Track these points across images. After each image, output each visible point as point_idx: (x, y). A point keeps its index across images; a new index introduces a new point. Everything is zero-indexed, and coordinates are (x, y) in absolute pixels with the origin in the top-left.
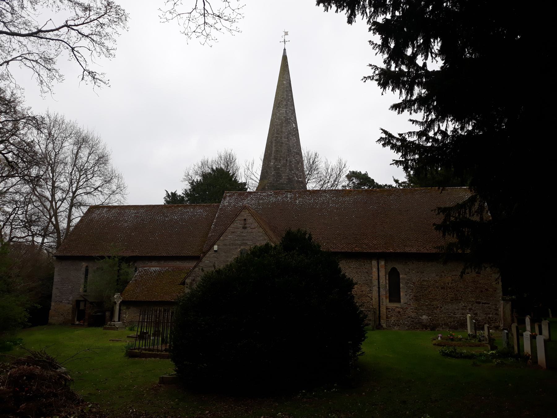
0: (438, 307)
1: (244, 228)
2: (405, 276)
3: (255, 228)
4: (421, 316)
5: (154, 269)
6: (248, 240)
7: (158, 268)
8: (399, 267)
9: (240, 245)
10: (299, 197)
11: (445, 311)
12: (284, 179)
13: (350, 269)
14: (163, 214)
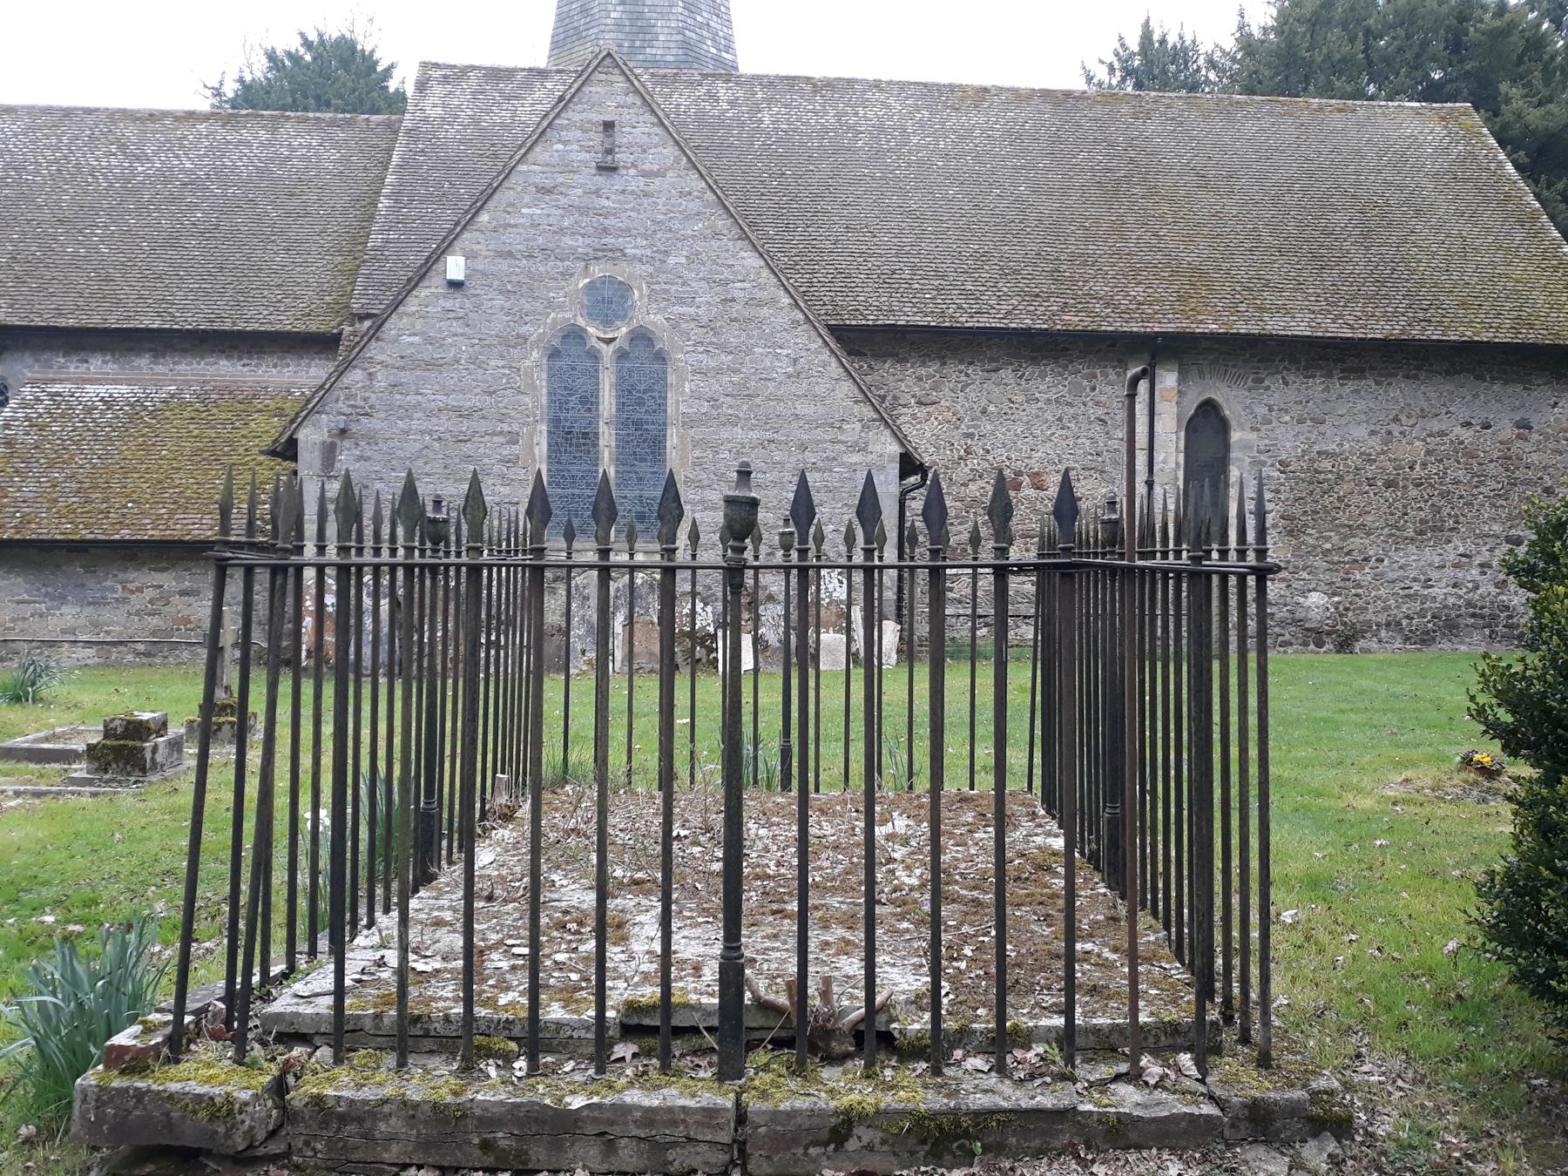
0: (1366, 559)
2: (1254, 435)
3: (660, 174)
4: (1304, 593)
5: (102, 390)
6: (626, 232)
7: (124, 389)
8: (1232, 399)
9: (587, 260)
10: (769, 101)
11: (1392, 575)
12: (664, 46)
13: (1033, 409)
14: (123, 147)
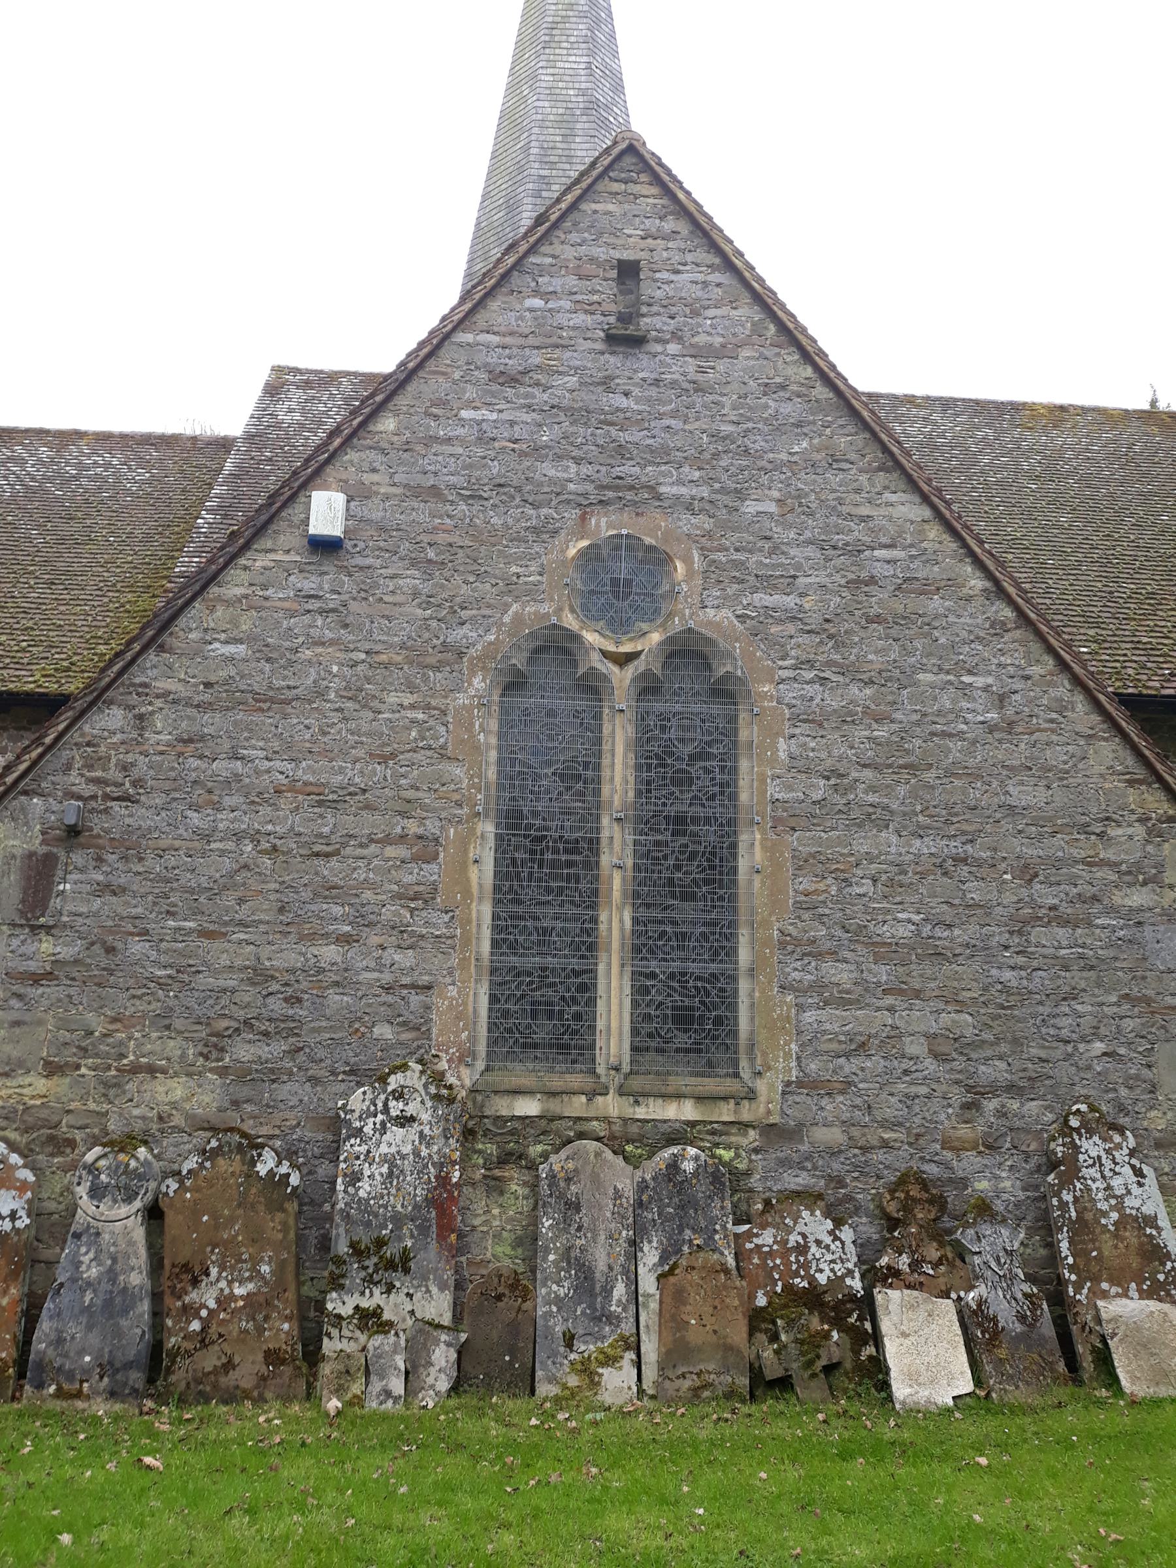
1: (625, 339)
6: (661, 455)
9: (585, 508)
